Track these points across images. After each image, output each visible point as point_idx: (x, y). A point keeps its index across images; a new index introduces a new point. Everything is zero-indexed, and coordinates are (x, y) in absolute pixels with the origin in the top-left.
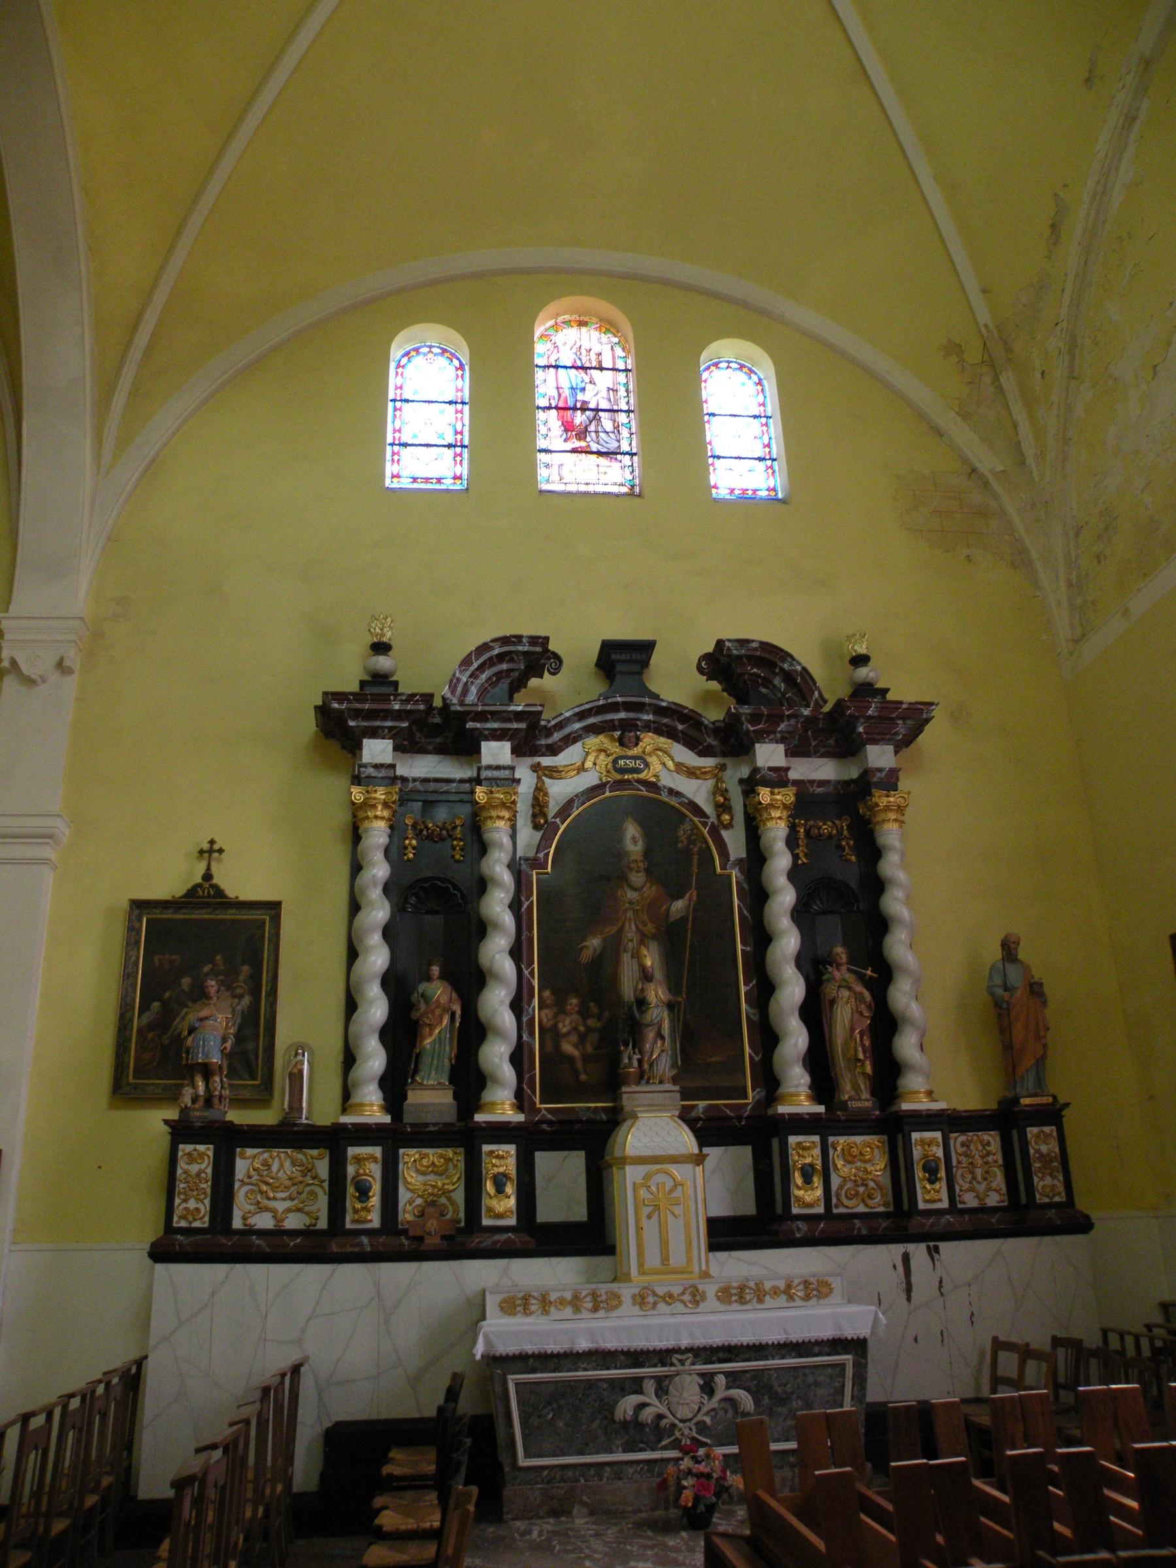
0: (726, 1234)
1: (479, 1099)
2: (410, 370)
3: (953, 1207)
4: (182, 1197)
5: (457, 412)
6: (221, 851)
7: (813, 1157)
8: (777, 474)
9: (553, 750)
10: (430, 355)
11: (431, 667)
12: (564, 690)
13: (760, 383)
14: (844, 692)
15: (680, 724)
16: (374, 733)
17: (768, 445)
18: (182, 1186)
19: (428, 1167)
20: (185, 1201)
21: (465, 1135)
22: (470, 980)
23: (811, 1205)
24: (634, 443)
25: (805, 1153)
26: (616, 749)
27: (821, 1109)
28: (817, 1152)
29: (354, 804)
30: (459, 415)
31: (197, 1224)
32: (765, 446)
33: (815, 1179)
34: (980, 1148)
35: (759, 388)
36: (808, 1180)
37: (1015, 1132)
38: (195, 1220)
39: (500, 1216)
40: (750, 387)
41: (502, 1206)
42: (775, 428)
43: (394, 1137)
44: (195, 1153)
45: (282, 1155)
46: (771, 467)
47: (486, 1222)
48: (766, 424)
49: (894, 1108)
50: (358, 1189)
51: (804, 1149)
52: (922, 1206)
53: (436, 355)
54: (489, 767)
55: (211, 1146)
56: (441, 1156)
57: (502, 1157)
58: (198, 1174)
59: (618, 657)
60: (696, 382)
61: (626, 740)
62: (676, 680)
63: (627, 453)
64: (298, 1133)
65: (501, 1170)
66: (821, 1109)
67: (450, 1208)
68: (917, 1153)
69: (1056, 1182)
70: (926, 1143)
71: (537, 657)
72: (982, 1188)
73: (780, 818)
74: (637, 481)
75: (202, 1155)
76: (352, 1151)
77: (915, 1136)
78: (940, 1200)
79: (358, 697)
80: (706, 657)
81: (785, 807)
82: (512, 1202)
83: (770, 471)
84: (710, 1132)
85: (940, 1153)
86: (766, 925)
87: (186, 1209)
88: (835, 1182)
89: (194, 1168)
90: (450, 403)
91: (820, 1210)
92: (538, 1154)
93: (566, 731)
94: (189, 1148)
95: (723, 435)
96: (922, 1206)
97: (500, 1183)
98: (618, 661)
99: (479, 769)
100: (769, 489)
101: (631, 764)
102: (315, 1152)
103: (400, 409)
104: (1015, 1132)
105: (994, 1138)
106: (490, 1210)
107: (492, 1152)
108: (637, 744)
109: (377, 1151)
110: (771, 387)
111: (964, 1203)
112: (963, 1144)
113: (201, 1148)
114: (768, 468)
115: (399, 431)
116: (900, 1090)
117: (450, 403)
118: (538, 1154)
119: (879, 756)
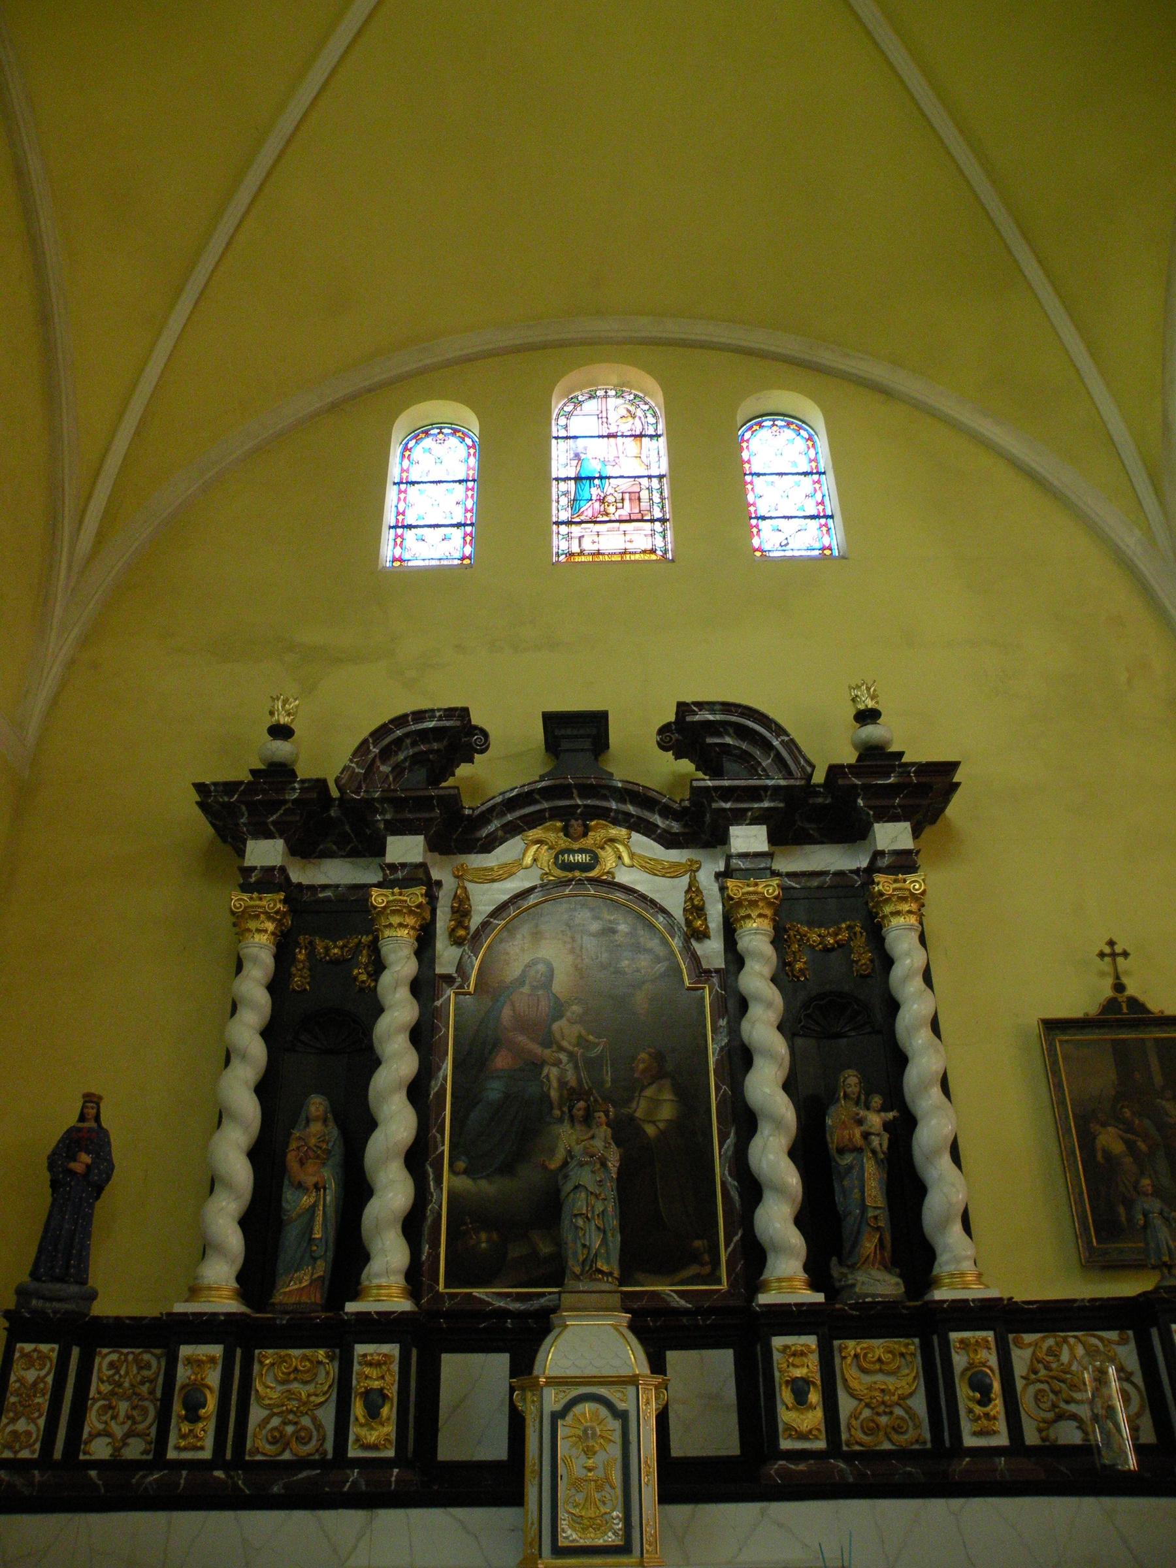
0: (689, 1481)
1: (358, 1282)
2: (418, 452)
3: (158, 1459)
4: (11, 1415)
5: (814, 482)
6: (1111, 943)
7: (808, 1368)
8: (832, 531)
9: (488, 846)
10: (441, 436)
11: (326, 753)
12: (488, 777)
13: (810, 438)
14: (849, 756)
15: (639, 808)
16: (739, 817)
17: (822, 503)
18: (13, 1399)
19: (874, 1363)
20: (13, 1421)
21: (334, 1329)
22: (357, 1124)
23: (375, 1447)
24: (667, 509)
25: (797, 1361)
26: (563, 842)
27: (820, 1298)
28: (813, 1360)
29: (233, 913)
30: (817, 486)
31: (25, 1454)
32: (818, 504)
33: (385, 1411)
34: (135, 1370)
35: (810, 443)
36: (800, 1398)
37: (1154, 1332)
38: (21, 1449)
39: (803, 1436)
40: (800, 444)
41: (375, 1436)
42: (828, 482)
43: (241, 1336)
44: (35, 1355)
45: (1072, 1341)
46: (826, 525)
47: (785, 1444)
48: (819, 482)
49: (927, 1298)
50: (186, 1406)
51: (795, 1355)
52: (969, 1441)
53: (781, 427)
54: (744, 856)
55: (56, 1346)
56: (305, 1358)
57: (803, 1354)
58: (35, 1384)
59: (563, 732)
60: (737, 445)
61: (571, 830)
62: (639, 756)
63: (658, 520)
64: (394, 1319)
65: (376, 1384)
66: (820, 1298)
67: (315, 1433)
68: (959, 1360)
69: (32, 1428)
70: (971, 1350)
71: (458, 737)
72: (118, 1431)
73: (910, 912)
74: (669, 547)
75: (43, 1357)
76: (185, 1351)
77: (954, 1336)
78: (202, 1448)
79: (251, 788)
80: (664, 730)
81: (770, 904)
82: (390, 1429)
83: (824, 529)
84: (658, 1332)
85: (993, 1361)
86: (900, 1045)
87: (14, 1432)
88: (846, 1406)
89: (31, 1375)
90: (460, 482)
91: (821, 1445)
92: (507, 1355)
93: (646, 815)
94: (28, 1347)
95: (765, 496)
96: (969, 1441)
97: (373, 1402)
98: (564, 737)
99: (729, 857)
100: (824, 548)
101: (580, 858)
102: (1113, 1335)
103: (405, 492)
104: (1154, 1332)
105: (158, 1358)
106: (358, 1440)
107: (786, 1347)
108: (585, 835)
109: (811, 1341)
110: (822, 443)
111: (89, 1453)
112: (112, 1365)
113: (44, 1348)
114: (821, 526)
115: (403, 514)
116: (365, 1283)
117: (460, 482)
118: (507, 1355)
119: (892, 835)
